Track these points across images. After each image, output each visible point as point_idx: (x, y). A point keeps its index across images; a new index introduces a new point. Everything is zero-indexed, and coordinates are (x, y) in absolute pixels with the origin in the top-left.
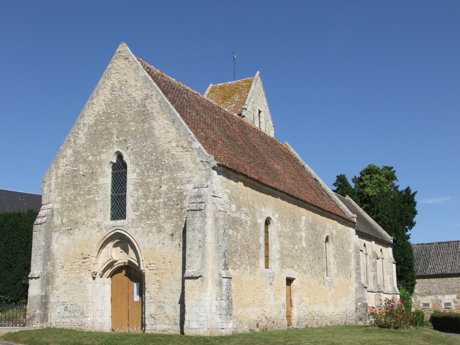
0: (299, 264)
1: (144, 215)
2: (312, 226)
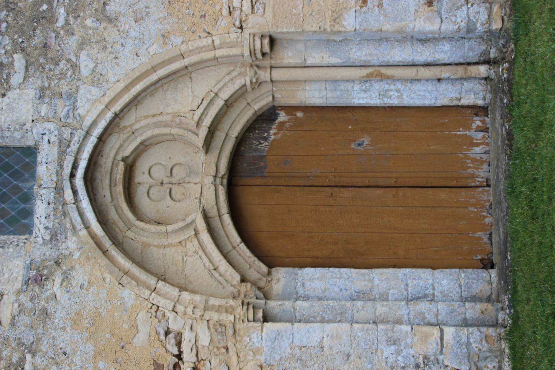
1: (30, 38)
2: (339, 271)
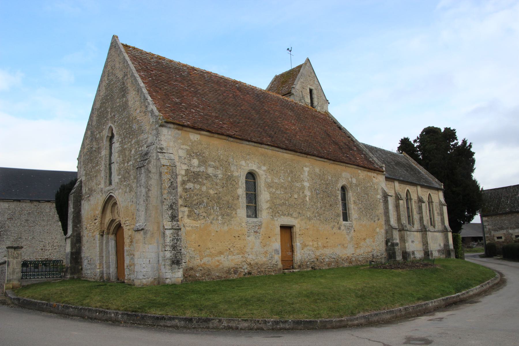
0: (301, 212)
